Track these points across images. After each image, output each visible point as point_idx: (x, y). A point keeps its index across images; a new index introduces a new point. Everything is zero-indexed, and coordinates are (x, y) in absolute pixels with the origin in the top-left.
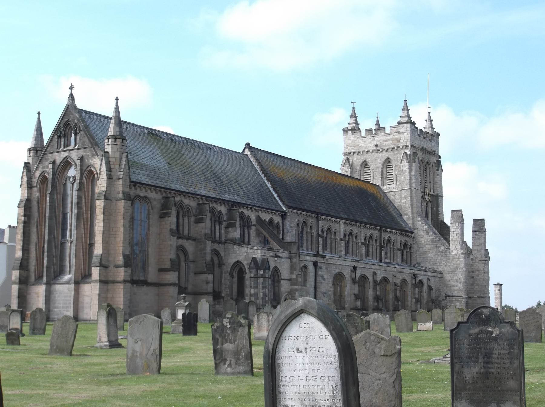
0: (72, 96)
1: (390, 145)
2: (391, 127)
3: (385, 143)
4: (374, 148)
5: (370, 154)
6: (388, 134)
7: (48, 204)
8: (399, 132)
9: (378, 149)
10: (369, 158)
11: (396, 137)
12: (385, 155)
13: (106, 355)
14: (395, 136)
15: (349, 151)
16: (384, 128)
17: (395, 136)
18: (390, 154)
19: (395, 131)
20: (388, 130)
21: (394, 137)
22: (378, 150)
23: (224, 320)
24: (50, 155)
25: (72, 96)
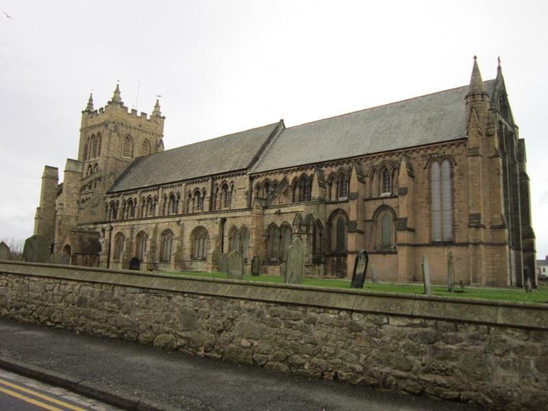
20: (148, 118)
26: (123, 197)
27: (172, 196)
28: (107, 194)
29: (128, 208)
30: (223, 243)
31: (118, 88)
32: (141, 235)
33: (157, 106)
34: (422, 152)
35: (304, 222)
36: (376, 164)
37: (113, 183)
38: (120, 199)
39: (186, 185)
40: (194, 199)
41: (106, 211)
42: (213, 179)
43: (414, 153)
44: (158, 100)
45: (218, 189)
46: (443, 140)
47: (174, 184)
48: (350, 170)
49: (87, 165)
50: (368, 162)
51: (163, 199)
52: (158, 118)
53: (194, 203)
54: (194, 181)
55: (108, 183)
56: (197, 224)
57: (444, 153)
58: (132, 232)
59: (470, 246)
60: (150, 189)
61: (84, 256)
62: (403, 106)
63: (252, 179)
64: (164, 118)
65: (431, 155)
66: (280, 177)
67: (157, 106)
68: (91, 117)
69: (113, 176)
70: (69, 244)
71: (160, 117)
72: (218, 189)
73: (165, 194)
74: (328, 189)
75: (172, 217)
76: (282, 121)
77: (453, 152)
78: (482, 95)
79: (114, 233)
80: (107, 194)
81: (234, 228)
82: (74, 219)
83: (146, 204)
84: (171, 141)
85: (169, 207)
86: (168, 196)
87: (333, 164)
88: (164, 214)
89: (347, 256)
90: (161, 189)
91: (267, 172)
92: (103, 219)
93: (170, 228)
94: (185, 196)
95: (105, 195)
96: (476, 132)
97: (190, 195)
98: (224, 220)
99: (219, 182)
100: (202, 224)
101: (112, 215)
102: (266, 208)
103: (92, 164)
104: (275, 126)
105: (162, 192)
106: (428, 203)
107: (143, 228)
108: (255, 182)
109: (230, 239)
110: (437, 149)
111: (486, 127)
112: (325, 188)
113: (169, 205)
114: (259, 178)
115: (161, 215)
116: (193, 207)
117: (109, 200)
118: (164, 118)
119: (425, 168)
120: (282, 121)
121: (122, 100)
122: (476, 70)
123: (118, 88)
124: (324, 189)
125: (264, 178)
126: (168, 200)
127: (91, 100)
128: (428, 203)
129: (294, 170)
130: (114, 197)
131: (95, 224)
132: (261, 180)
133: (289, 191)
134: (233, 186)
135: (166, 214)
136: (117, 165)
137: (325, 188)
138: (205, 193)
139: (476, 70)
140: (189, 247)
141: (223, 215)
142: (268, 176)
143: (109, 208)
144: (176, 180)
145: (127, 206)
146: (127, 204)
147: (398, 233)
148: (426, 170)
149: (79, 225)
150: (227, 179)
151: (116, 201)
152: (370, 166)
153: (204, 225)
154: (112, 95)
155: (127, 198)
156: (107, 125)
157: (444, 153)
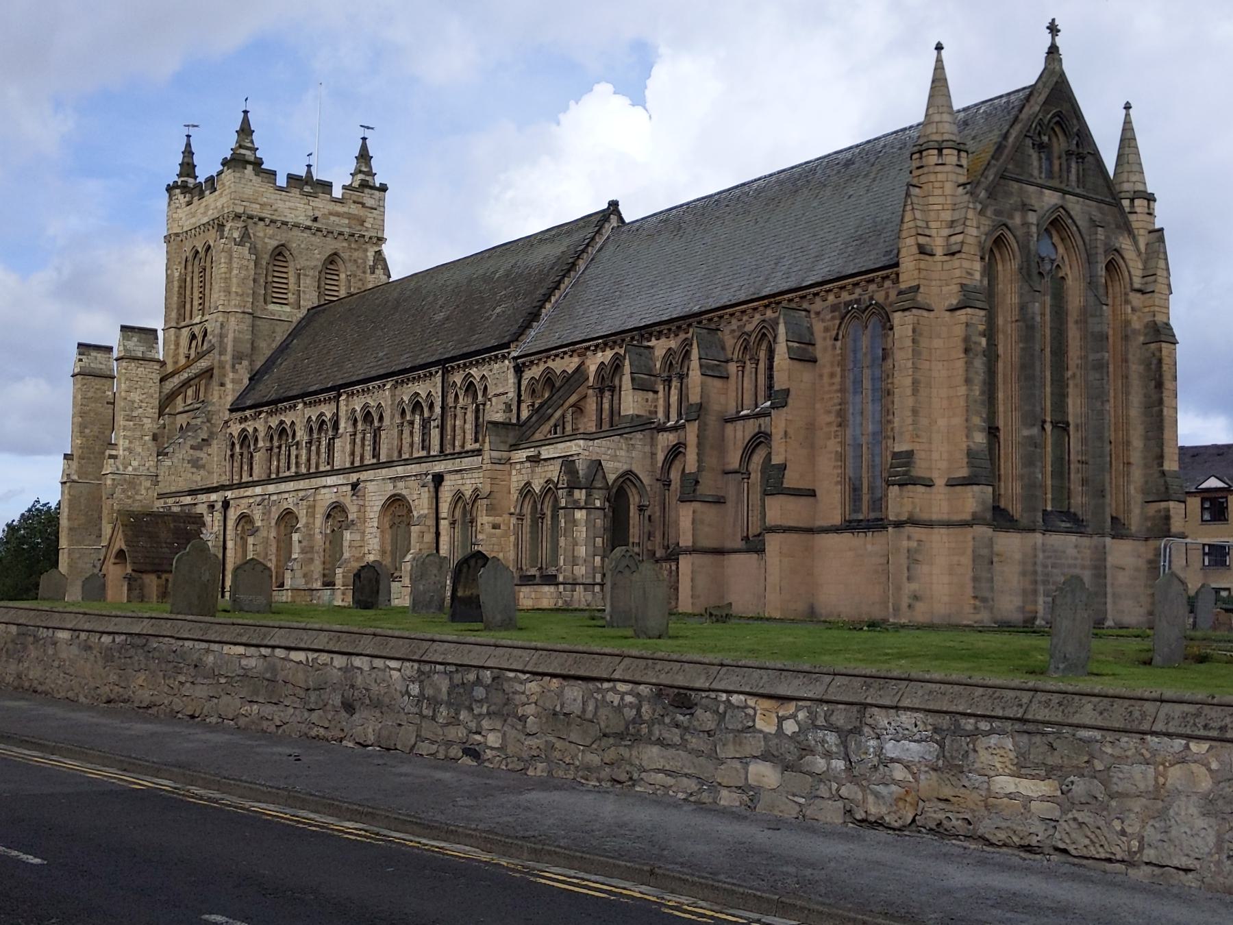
0: (1053, 51)
1: (342, 224)
2: (344, 187)
3: (332, 218)
4: (309, 223)
5: (296, 232)
6: (336, 201)
7: (24, 857)
8: (363, 205)
9: (314, 227)
10: (297, 240)
11: (356, 212)
12: (332, 245)
13: (916, 353)
14: (354, 209)
15: (274, 217)
16: (274, 173)
17: (354, 209)
18: (340, 245)
19: (354, 198)
20: (337, 192)
21: (351, 211)
22: (319, 230)
23: (393, 584)
24: (1016, 185)
25: (1053, 51)
26: (266, 419)
27: (368, 417)
28: (231, 411)
29: (280, 447)
30: (438, 534)
31: (246, 122)
32: (288, 517)
33: (364, 156)
34: (831, 297)
35: (583, 481)
36: (749, 328)
37: (246, 382)
38: (260, 425)
39: (395, 387)
40: (412, 423)
41: (232, 456)
42: (446, 372)
43: (818, 299)
44: (364, 139)
45: (456, 395)
46: (781, 289)
47: (370, 385)
48: (775, 323)
49: (185, 332)
50: (735, 324)
51: (351, 422)
52: (366, 185)
53: (412, 433)
54: (411, 375)
55: (233, 381)
56: (389, 489)
57: (871, 298)
58: (267, 512)
59: (890, 529)
60: (321, 397)
61: (159, 577)
62: (759, 192)
63: (519, 371)
64: (383, 188)
65: (847, 304)
66: (570, 364)
67: (364, 156)
68: (189, 203)
69: (245, 363)
70: (124, 547)
71: (373, 188)
72: (456, 395)
73: (354, 411)
74: (661, 394)
75: (419, 460)
76: (614, 205)
77: (887, 296)
78: (940, 150)
79: (233, 515)
80: (231, 411)
81: (458, 497)
82: (148, 484)
83: (315, 436)
84: (408, 251)
85: (363, 445)
86: (359, 415)
87: (679, 328)
88: (352, 463)
89: (677, 560)
90: (344, 397)
91: (547, 353)
92: (225, 480)
93: (342, 499)
94: (393, 417)
95: (227, 415)
96: (915, 250)
97: (403, 412)
98: (438, 479)
99: (458, 378)
100: (401, 487)
101: (245, 468)
102: (515, 447)
103: (196, 329)
104: (598, 217)
105: (393, 396)
106: (840, 425)
107: (290, 503)
108: (527, 375)
109: (1128, 443)
110: (858, 291)
111: (946, 232)
112: (656, 392)
113: (363, 439)
114: (534, 368)
115: (348, 465)
116: (412, 445)
117: (235, 429)
118: (383, 188)
119: (836, 339)
120: (614, 205)
121: (259, 154)
122: (939, 82)
123: (246, 122)
124: (651, 395)
125: (542, 367)
126: (360, 427)
127: (188, 152)
128: (840, 425)
129: (597, 346)
130: (246, 419)
131: (192, 492)
132: (535, 372)
133: (589, 400)
134: (486, 387)
135: (357, 464)
136: (304, 320)
137: (656, 392)
138: (431, 406)
139: (939, 82)
140: (377, 547)
141: (439, 467)
142: (550, 364)
143: (237, 447)
144: (373, 373)
145: (276, 444)
146: (276, 438)
147: (768, 500)
148: (839, 344)
149: (161, 496)
150: (474, 371)
151: (250, 430)
152: (737, 334)
153: (404, 492)
154: (232, 140)
155: (357, 404)
156: (221, 226)
157: (871, 298)
